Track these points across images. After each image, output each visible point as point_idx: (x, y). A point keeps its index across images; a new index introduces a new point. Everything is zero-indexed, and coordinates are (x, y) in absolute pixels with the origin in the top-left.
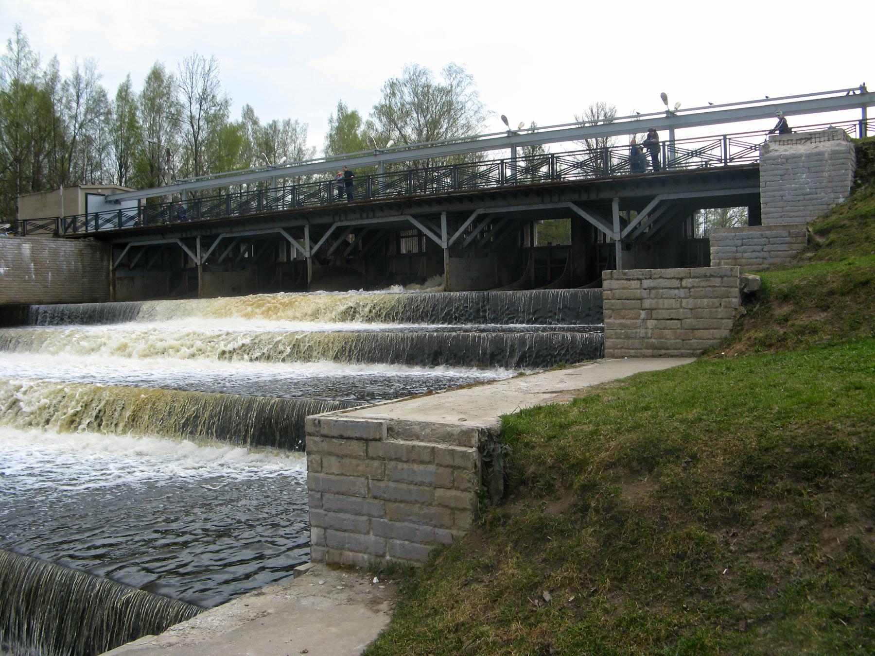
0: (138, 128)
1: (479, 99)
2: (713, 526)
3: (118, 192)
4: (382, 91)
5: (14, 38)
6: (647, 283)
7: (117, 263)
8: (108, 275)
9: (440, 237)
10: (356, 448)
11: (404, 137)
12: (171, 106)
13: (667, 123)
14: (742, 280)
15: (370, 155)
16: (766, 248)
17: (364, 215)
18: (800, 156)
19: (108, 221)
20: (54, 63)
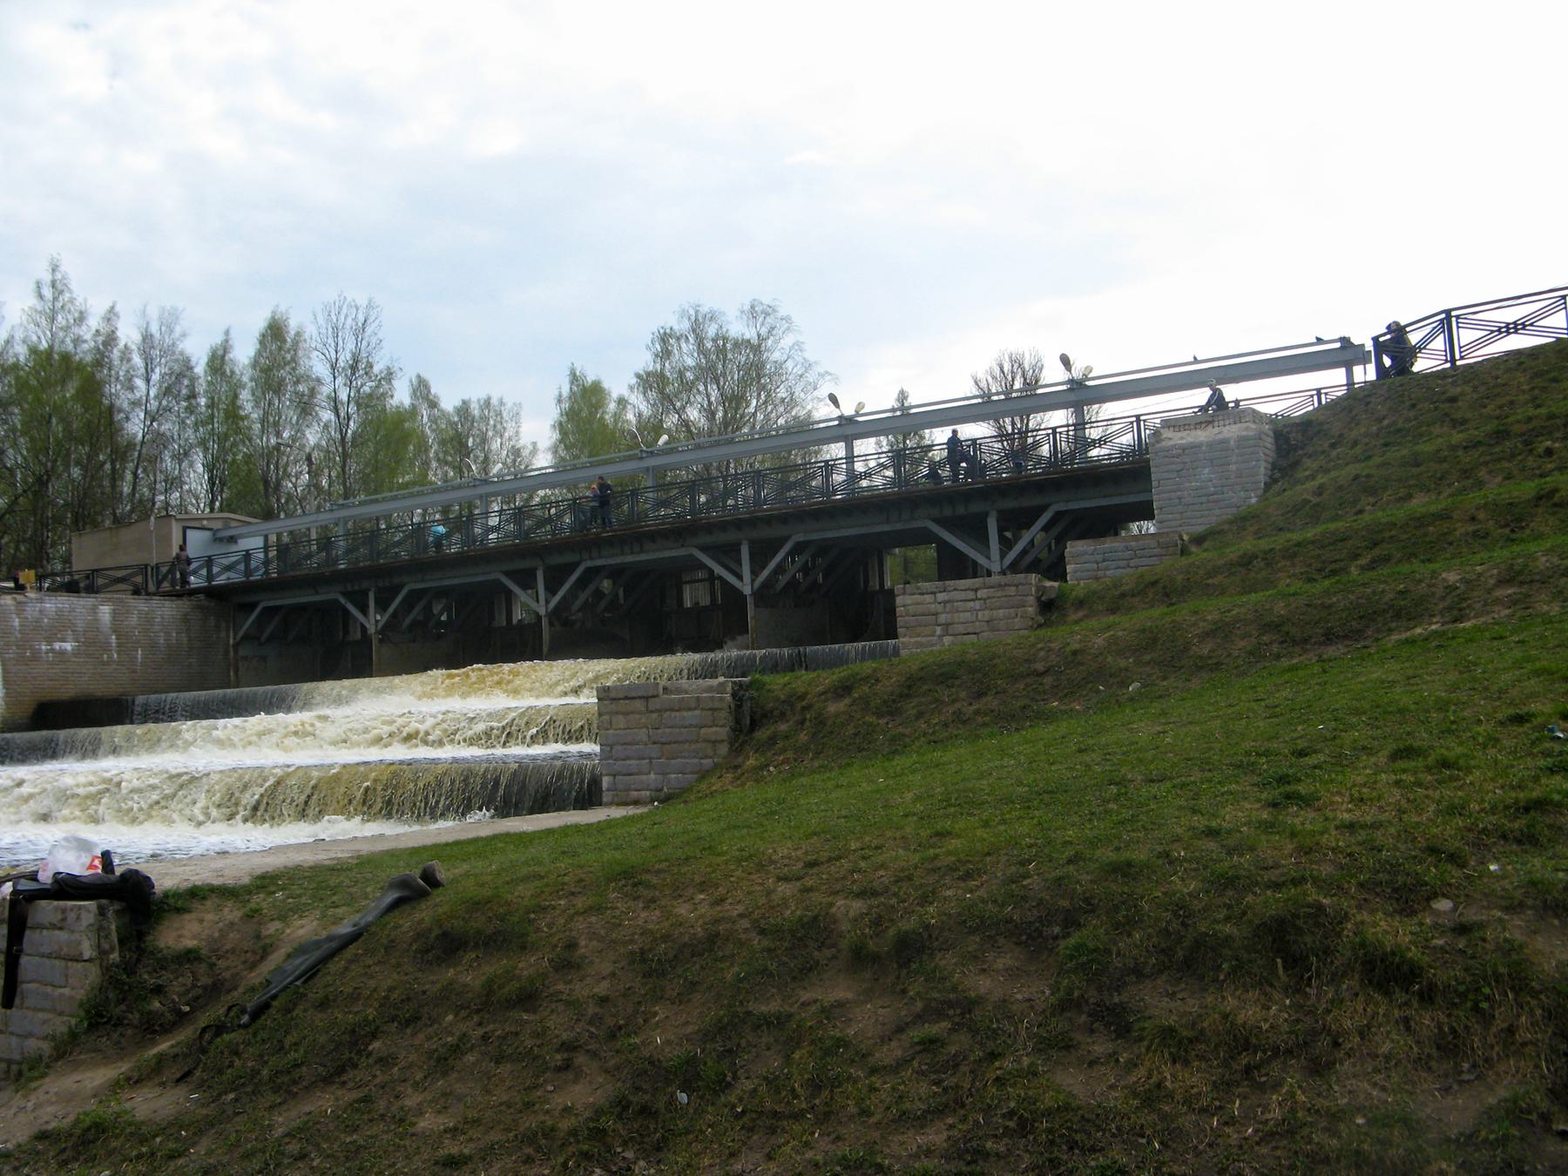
0: (243, 419)
1: (806, 355)
2: (880, 715)
3: (233, 524)
4: (648, 348)
5: (47, 278)
6: (941, 597)
7: (241, 633)
8: (227, 652)
9: (740, 578)
10: (639, 705)
11: (686, 424)
12: (298, 382)
13: (1072, 397)
14: (1038, 590)
15: (630, 458)
16: (1132, 563)
18: (1199, 446)
20: (111, 315)
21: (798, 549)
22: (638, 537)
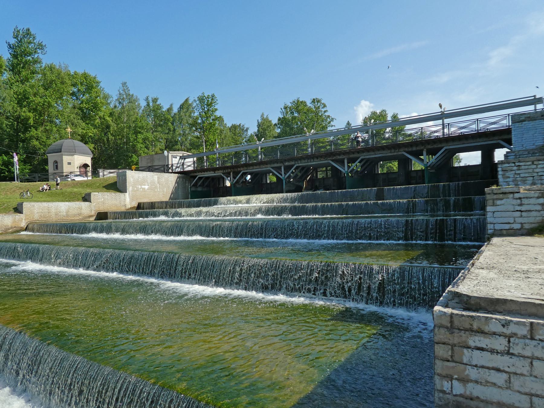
17: (309, 161)
19: (189, 166)
21: (297, 168)
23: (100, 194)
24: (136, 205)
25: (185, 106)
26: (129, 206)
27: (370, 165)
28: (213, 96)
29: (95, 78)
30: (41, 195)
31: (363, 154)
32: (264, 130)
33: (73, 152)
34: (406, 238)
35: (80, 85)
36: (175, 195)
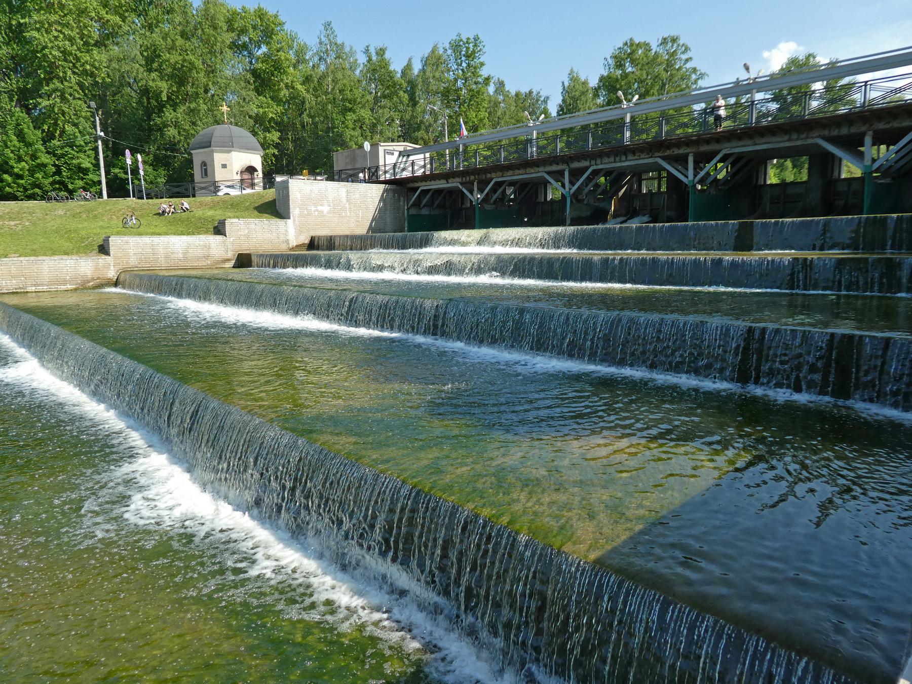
17: (618, 159)
22: (623, 151)
23: (242, 221)
24: (307, 241)
25: (433, 61)
26: (294, 243)
27: (748, 169)
28: (476, 39)
29: (276, 16)
30: (158, 221)
31: (728, 145)
32: (575, 99)
33: (229, 145)
34: (743, 377)
35: (251, 30)
36: (377, 226)
